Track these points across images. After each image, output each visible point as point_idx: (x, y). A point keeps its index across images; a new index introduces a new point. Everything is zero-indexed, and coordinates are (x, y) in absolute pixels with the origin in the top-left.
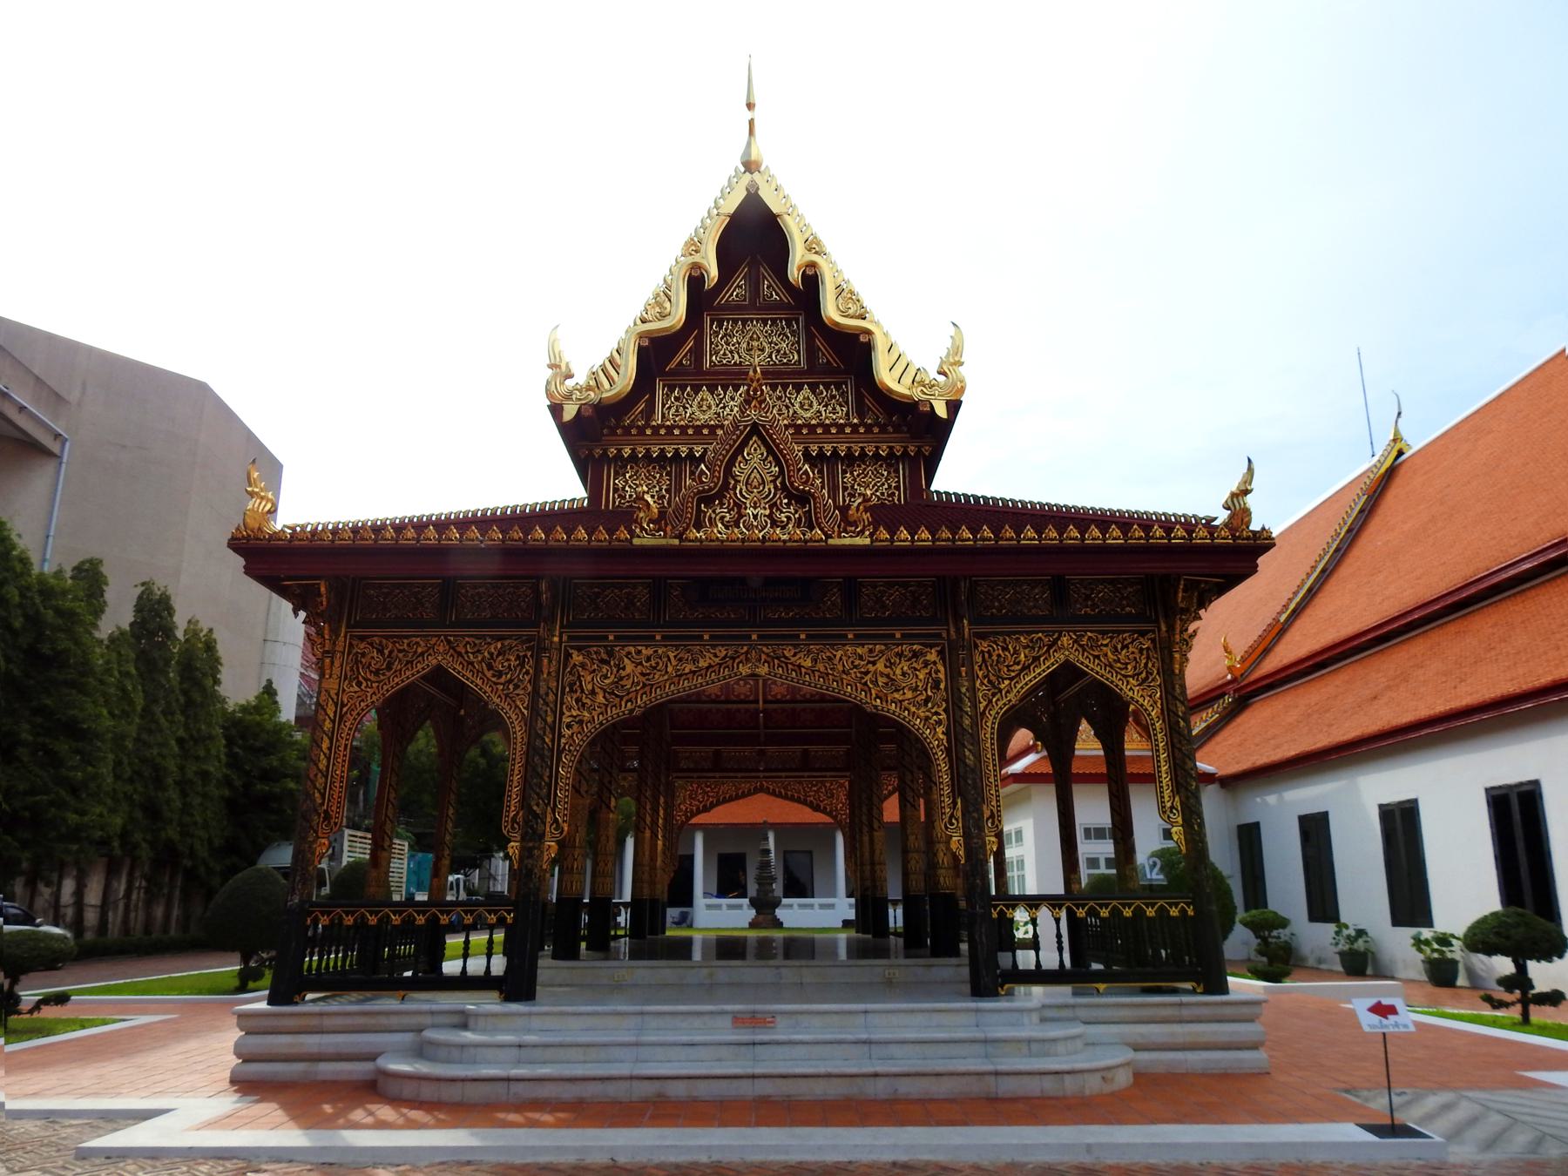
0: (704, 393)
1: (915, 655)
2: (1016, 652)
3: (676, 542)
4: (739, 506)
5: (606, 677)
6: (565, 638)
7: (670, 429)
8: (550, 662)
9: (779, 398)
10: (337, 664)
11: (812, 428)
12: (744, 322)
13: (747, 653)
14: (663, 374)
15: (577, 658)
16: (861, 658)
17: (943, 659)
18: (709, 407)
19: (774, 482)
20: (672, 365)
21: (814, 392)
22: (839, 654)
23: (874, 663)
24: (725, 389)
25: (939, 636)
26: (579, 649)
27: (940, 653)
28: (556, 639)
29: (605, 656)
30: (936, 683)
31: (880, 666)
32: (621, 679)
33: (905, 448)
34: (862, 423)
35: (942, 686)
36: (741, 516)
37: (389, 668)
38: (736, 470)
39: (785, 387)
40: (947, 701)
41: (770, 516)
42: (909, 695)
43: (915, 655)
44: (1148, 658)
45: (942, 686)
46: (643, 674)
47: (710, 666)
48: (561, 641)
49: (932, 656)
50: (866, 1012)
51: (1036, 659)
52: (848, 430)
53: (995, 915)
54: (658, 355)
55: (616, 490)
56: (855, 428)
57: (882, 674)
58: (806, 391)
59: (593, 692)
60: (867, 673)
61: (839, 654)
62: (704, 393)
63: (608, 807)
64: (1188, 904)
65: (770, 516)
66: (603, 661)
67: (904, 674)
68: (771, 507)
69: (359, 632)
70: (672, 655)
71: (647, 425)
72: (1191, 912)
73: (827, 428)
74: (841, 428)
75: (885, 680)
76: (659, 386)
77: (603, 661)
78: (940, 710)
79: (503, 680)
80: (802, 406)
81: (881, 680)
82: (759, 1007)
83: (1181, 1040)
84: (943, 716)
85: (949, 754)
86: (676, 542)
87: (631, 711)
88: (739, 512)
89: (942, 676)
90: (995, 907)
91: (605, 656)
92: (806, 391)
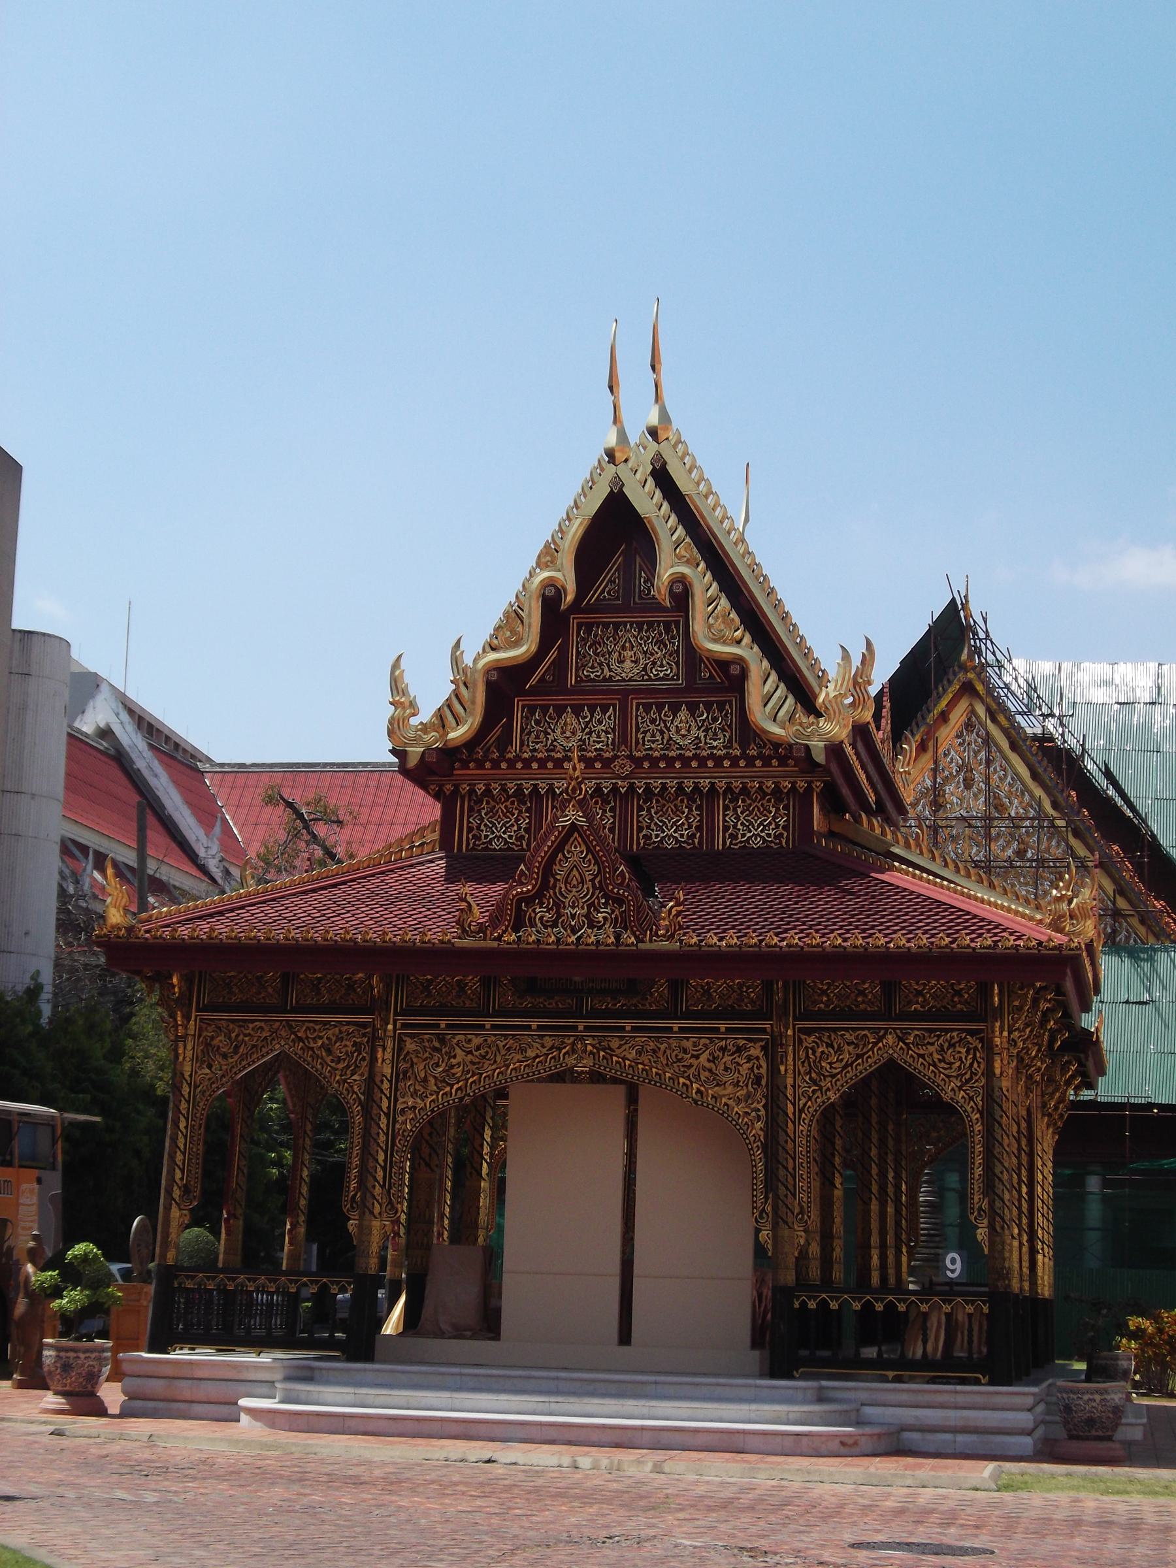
0: (569, 718)
1: (739, 1050)
2: (839, 1050)
3: (495, 944)
4: (558, 905)
5: (437, 1065)
6: (398, 1025)
7: (527, 763)
8: (384, 1049)
9: (653, 721)
10: (189, 1047)
11: (685, 761)
12: (617, 626)
13: (573, 1044)
14: (522, 693)
15: (410, 1045)
16: (685, 1051)
17: (766, 1054)
18: (573, 733)
19: (592, 880)
20: (533, 681)
21: (693, 715)
22: (663, 1047)
23: (697, 1057)
24: (592, 710)
25: (764, 1031)
26: (412, 1036)
27: (764, 1048)
28: (390, 1027)
29: (437, 1044)
30: (758, 1079)
31: (703, 1059)
32: (452, 1067)
33: (793, 784)
34: (744, 756)
35: (764, 1082)
36: (559, 916)
37: (236, 1051)
38: (556, 868)
39: (660, 707)
40: (766, 1097)
41: (587, 916)
42: (730, 1089)
43: (739, 1050)
44: (974, 1058)
45: (764, 1082)
46: (472, 1063)
47: (537, 1056)
48: (395, 1029)
49: (756, 1051)
50: (656, 1383)
51: (858, 1056)
52: (726, 763)
53: (797, 1305)
54: (504, 687)
55: (470, 830)
56: (735, 761)
57: (704, 1068)
58: (683, 714)
59: (425, 1080)
60: (691, 1066)
61: (663, 1047)
62: (569, 718)
63: (372, 1213)
64: (984, 1303)
65: (587, 916)
66: (435, 1049)
67: (726, 1069)
68: (589, 907)
69: (207, 1016)
70: (501, 1044)
71: (502, 758)
72: (986, 1310)
73: (702, 761)
74: (718, 761)
75: (707, 1074)
76: (518, 704)
77: (435, 1049)
78: (760, 1106)
79: (341, 1066)
80: (678, 730)
81: (704, 1075)
82: (163, 1186)
83: (952, 1423)
84: (762, 1113)
85: (765, 1151)
86: (495, 944)
87: (461, 1099)
88: (558, 912)
89: (763, 1071)
90: (798, 1297)
91: (437, 1044)
92: (683, 714)
